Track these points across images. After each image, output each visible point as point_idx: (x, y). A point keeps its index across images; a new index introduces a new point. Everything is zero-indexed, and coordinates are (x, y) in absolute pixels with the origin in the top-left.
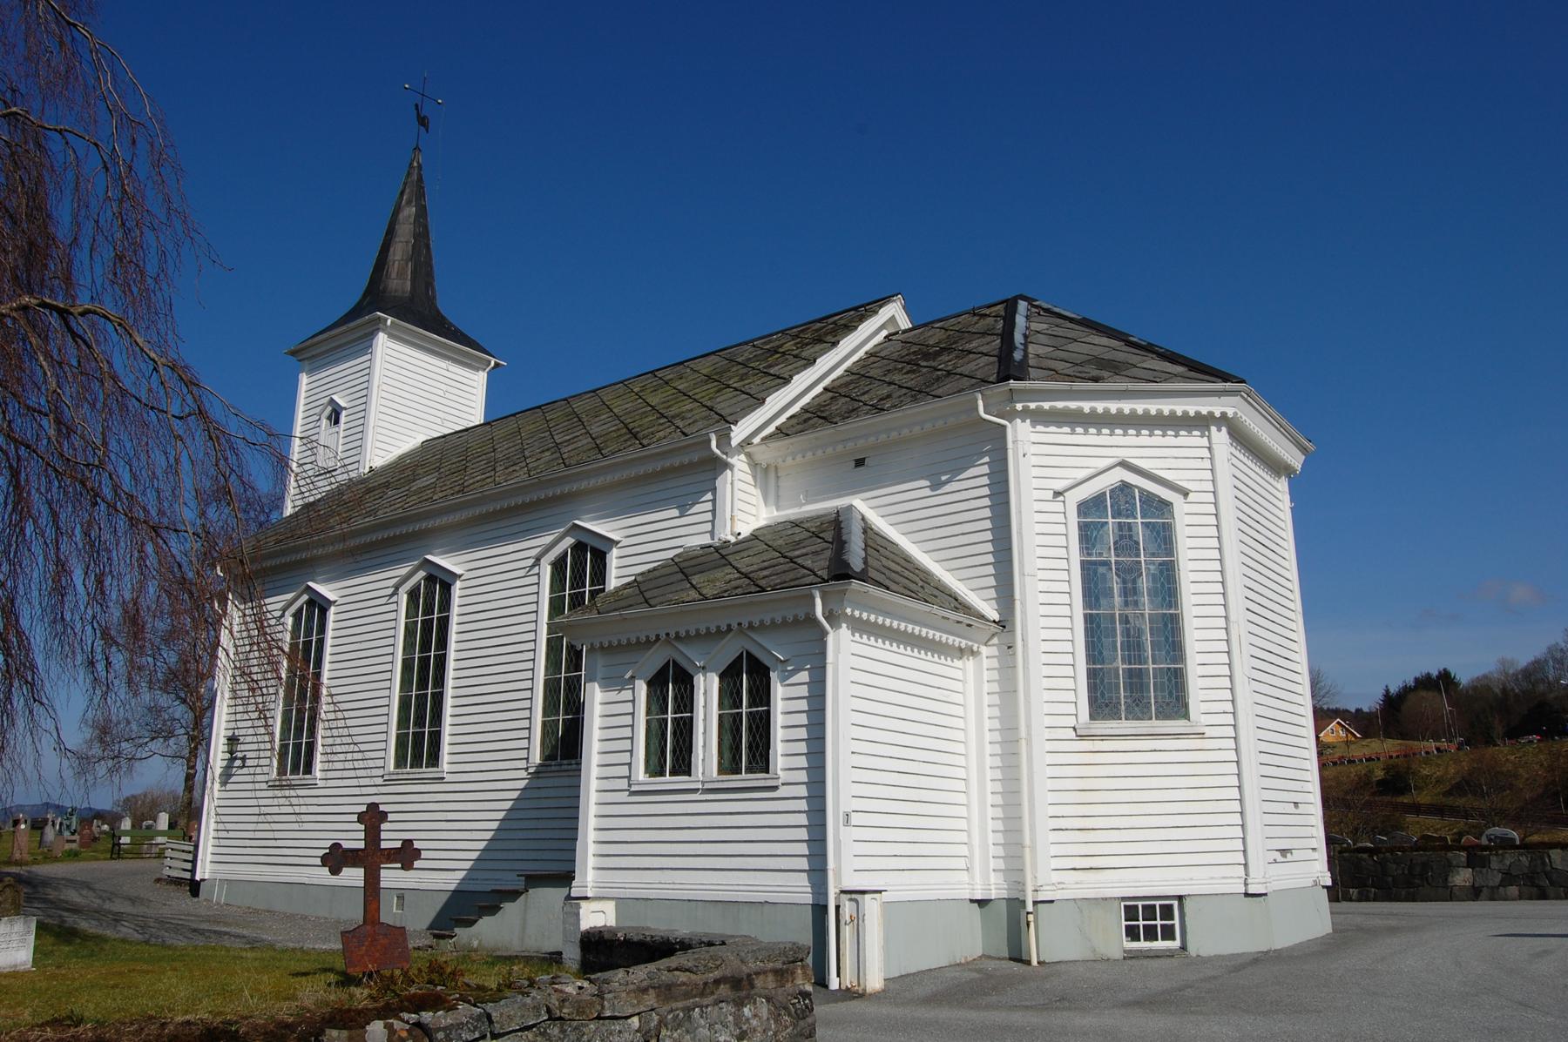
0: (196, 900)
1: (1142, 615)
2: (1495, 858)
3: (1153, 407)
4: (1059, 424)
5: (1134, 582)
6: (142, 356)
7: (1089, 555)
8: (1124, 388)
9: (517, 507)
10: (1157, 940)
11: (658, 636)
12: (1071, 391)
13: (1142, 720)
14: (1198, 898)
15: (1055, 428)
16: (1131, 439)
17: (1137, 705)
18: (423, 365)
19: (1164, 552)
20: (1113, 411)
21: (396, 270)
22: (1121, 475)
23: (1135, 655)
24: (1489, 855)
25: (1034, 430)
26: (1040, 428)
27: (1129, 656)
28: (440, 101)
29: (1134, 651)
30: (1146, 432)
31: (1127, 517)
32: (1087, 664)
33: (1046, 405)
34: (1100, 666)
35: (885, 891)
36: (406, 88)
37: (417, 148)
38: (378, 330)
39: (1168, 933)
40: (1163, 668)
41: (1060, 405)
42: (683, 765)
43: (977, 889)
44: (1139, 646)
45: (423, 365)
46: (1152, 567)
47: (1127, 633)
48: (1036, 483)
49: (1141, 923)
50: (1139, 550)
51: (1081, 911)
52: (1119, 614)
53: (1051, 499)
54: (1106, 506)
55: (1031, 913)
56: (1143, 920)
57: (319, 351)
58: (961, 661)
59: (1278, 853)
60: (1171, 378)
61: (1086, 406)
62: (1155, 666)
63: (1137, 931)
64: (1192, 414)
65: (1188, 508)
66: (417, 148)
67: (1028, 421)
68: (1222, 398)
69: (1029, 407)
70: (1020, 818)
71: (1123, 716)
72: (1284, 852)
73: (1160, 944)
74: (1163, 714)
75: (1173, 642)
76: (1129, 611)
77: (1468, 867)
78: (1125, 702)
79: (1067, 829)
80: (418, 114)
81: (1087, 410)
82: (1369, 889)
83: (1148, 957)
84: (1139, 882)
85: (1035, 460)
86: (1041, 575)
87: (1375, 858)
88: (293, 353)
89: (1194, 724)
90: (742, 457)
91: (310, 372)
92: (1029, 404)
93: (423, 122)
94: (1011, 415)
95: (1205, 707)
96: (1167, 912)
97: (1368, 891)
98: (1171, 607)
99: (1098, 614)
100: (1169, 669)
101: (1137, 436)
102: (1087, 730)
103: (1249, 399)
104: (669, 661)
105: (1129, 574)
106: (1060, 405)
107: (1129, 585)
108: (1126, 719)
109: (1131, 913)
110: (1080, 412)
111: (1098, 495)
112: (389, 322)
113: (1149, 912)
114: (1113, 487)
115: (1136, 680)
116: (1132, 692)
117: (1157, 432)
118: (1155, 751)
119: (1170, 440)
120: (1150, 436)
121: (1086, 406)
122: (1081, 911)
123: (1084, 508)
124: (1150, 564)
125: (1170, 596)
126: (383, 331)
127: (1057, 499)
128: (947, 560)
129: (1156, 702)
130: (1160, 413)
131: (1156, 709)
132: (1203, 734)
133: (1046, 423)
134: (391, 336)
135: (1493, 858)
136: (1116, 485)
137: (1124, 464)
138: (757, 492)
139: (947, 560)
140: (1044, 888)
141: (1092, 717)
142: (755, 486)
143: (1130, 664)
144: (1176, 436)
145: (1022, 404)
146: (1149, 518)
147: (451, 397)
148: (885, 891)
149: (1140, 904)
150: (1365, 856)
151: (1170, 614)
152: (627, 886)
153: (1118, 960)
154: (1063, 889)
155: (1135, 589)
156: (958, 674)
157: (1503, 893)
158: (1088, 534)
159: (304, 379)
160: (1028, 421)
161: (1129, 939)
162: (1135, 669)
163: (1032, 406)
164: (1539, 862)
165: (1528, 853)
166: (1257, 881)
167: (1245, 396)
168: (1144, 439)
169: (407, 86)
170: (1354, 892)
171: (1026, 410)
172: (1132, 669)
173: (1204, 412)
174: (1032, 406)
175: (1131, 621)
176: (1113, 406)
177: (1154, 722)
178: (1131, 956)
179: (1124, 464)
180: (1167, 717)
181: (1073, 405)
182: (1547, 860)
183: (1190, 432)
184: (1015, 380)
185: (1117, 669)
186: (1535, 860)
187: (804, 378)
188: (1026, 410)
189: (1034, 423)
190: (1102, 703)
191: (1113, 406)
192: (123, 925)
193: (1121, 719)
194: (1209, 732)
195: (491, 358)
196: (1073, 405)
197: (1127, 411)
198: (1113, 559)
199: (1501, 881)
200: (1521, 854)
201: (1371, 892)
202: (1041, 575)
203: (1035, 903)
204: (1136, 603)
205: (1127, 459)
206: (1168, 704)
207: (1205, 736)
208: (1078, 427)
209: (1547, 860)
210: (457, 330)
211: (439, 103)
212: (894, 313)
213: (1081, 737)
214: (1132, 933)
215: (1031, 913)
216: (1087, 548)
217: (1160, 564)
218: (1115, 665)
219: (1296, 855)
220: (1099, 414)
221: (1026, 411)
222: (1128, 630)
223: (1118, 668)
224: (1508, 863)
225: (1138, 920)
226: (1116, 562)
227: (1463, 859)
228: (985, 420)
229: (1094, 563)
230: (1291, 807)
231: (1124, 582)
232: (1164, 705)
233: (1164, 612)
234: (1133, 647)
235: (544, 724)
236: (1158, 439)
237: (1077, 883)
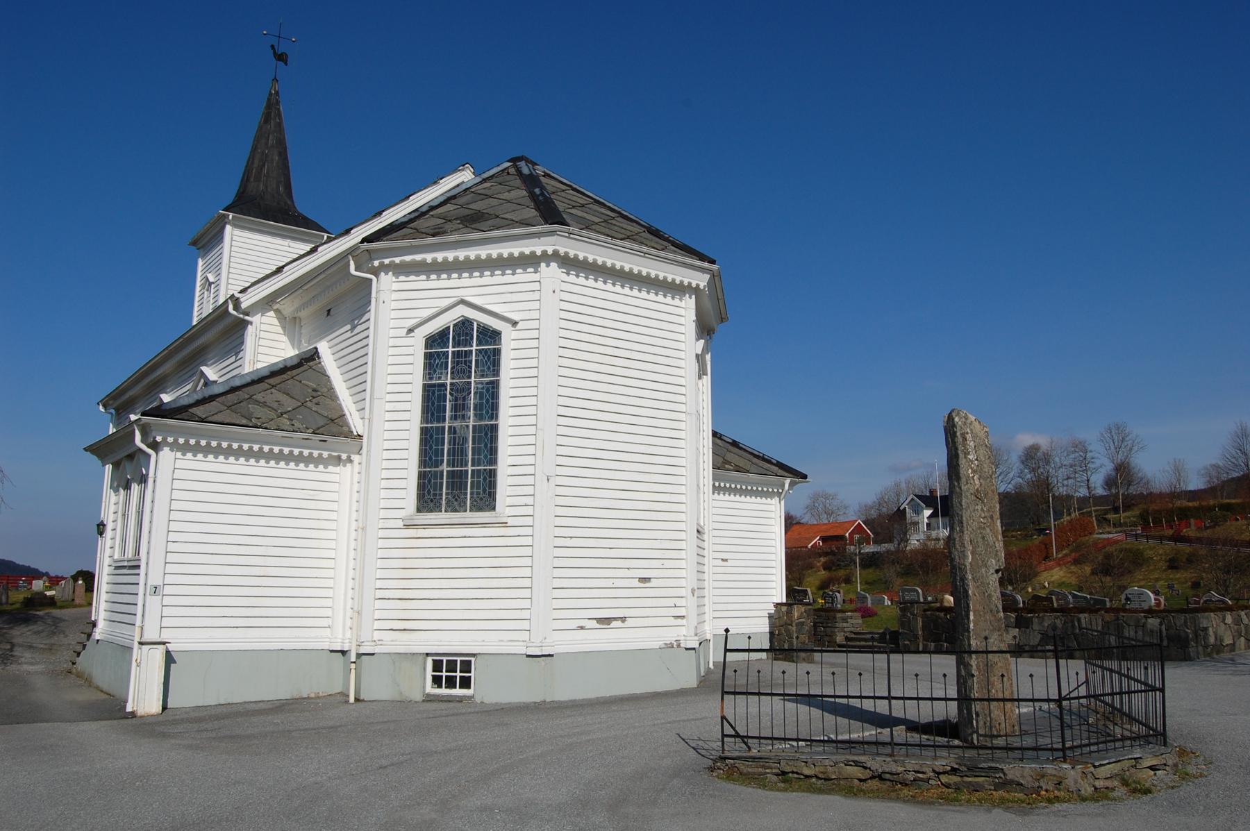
1: (467, 426)
2: (1036, 620)
3: (494, 251)
4: (417, 273)
5: (464, 399)
7: (431, 379)
8: (453, 239)
10: (455, 688)
12: (412, 247)
13: (458, 512)
14: (486, 657)
15: (413, 277)
16: (466, 280)
17: (456, 500)
18: (277, 247)
19: (492, 373)
20: (451, 259)
21: (253, 175)
22: (462, 312)
23: (458, 459)
24: (1032, 617)
25: (397, 280)
26: (402, 278)
27: (454, 460)
28: (294, 39)
29: (458, 456)
30: (488, 273)
31: (465, 346)
32: (419, 467)
33: (397, 260)
34: (429, 469)
35: (169, 643)
36: (265, 34)
37: (275, 79)
38: (226, 223)
39: (466, 683)
40: (480, 470)
41: (408, 258)
44: (463, 452)
45: (277, 247)
46: (480, 386)
47: (453, 441)
48: (393, 323)
49: (458, 674)
50: (471, 373)
51: (394, 663)
52: (449, 426)
53: (404, 335)
54: (449, 338)
55: (352, 662)
56: (461, 672)
57: (206, 240)
58: (339, 468)
60: (513, 224)
61: (429, 257)
62: (473, 468)
63: (454, 679)
64: (516, 255)
65: (515, 335)
66: (275, 79)
67: (390, 273)
68: (542, 238)
69: (384, 262)
70: (137, 594)
71: (443, 509)
73: (458, 691)
74: (477, 507)
76: (457, 424)
77: (1016, 627)
78: (446, 498)
79: (389, 599)
80: (275, 52)
81: (429, 261)
82: (942, 643)
83: (442, 701)
84: (441, 641)
85: (394, 305)
86: (389, 397)
87: (948, 617)
88: (194, 243)
89: (498, 515)
90: (272, 313)
91: (203, 257)
92: (384, 260)
93: (281, 58)
94: (376, 272)
95: (509, 501)
96: (466, 666)
97: (941, 645)
98: (492, 418)
99: (432, 427)
100: (485, 470)
101: (481, 277)
102: (411, 521)
105: (461, 392)
106: (408, 258)
107: (460, 402)
108: (446, 511)
109: (437, 666)
110: (423, 263)
111: (443, 330)
112: (231, 217)
113: (452, 666)
114: (456, 322)
115: (457, 480)
116: (452, 490)
117: (529, 270)
118: (465, 537)
119: (509, 278)
120: (503, 275)
121: (429, 257)
122: (394, 663)
123: (432, 341)
124: (479, 383)
125: (492, 410)
126: (229, 223)
127: (409, 336)
128: (355, 386)
129: (471, 497)
130: (500, 256)
131: (471, 503)
132: (506, 523)
133: (407, 274)
134: (235, 226)
135: (1035, 620)
136: (459, 320)
137: (463, 302)
138: (285, 338)
139: (355, 386)
140: (365, 644)
141: (419, 510)
142: (285, 335)
143: (453, 466)
144: (503, 275)
145: (378, 261)
146: (483, 345)
148: (169, 643)
149: (445, 659)
150: (942, 614)
151: (491, 424)
153: (418, 702)
154: (381, 645)
155: (464, 405)
156: (336, 478)
158: (432, 363)
159: (200, 262)
160: (390, 273)
161: (436, 686)
162: (457, 470)
163: (387, 261)
164: (1070, 625)
165: (1063, 616)
166: (534, 644)
168: (476, 280)
169: (265, 32)
170: (932, 646)
171: (382, 264)
172: (454, 471)
173: (527, 252)
174: (387, 261)
175: (458, 431)
176: (450, 255)
177: (468, 514)
178: (430, 699)
179: (463, 302)
180: (480, 509)
181: (418, 257)
182: (1076, 624)
183: (525, 270)
184: (367, 243)
185: (442, 472)
186: (1067, 623)
187: (337, 245)
188: (382, 264)
189: (397, 274)
190: (428, 498)
191: (450, 255)
193: (441, 511)
194: (511, 521)
195: (323, 234)
196: (418, 257)
197: (461, 258)
198: (449, 381)
199: (1040, 641)
200: (1056, 618)
201: (944, 645)
202: (389, 397)
203: (359, 655)
204: (463, 417)
205: (463, 298)
206: (481, 499)
207: (507, 525)
208: (432, 274)
209: (1076, 624)
210: (305, 218)
211: (294, 41)
212: (466, 176)
213: (407, 526)
214: (437, 681)
215: (352, 662)
216: (429, 374)
217: (487, 383)
218: (440, 468)
220: (471, 260)
221: (382, 266)
222: (455, 438)
223: (443, 470)
224: (1046, 625)
225: (456, 672)
226: (451, 384)
227: (1013, 620)
228: (355, 276)
229: (434, 385)
231: (456, 399)
232: (478, 500)
233: (486, 423)
234: (458, 453)
236: (487, 279)
237: (392, 641)
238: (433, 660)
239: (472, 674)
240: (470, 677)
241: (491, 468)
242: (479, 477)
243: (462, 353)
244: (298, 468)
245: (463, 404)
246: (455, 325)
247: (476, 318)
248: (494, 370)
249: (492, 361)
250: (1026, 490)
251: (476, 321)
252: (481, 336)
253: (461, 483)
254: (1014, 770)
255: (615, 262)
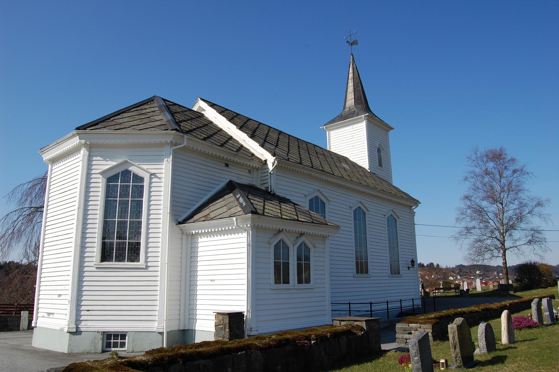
0: (446, 359)
6: (505, 236)
9: (342, 186)
11: (283, 229)
29: (126, 180)
42: (286, 281)
43: (187, 326)
59: (47, 314)
72: (49, 314)
74: (131, 260)
75: (137, 248)
103: (43, 152)
104: (281, 239)
147: (356, 136)
152: (141, 327)
157: (182, 327)
167: (42, 153)
192: (278, 148)
219: (55, 316)
230: (57, 297)
231: (122, 208)
234: (124, 204)
235: (142, 196)
238: (113, 348)
239: (126, 341)
240: (125, 342)
241: (141, 184)
242: (133, 224)
243: (121, 243)
244: (50, 317)
245: (125, 210)
246: (121, 172)
247: (133, 170)
248: (140, 195)
249: (139, 191)
250: (291, 339)
251: (132, 171)
252: (135, 179)
253: (125, 211)
254: (299, 258)
255: (206, 150)
